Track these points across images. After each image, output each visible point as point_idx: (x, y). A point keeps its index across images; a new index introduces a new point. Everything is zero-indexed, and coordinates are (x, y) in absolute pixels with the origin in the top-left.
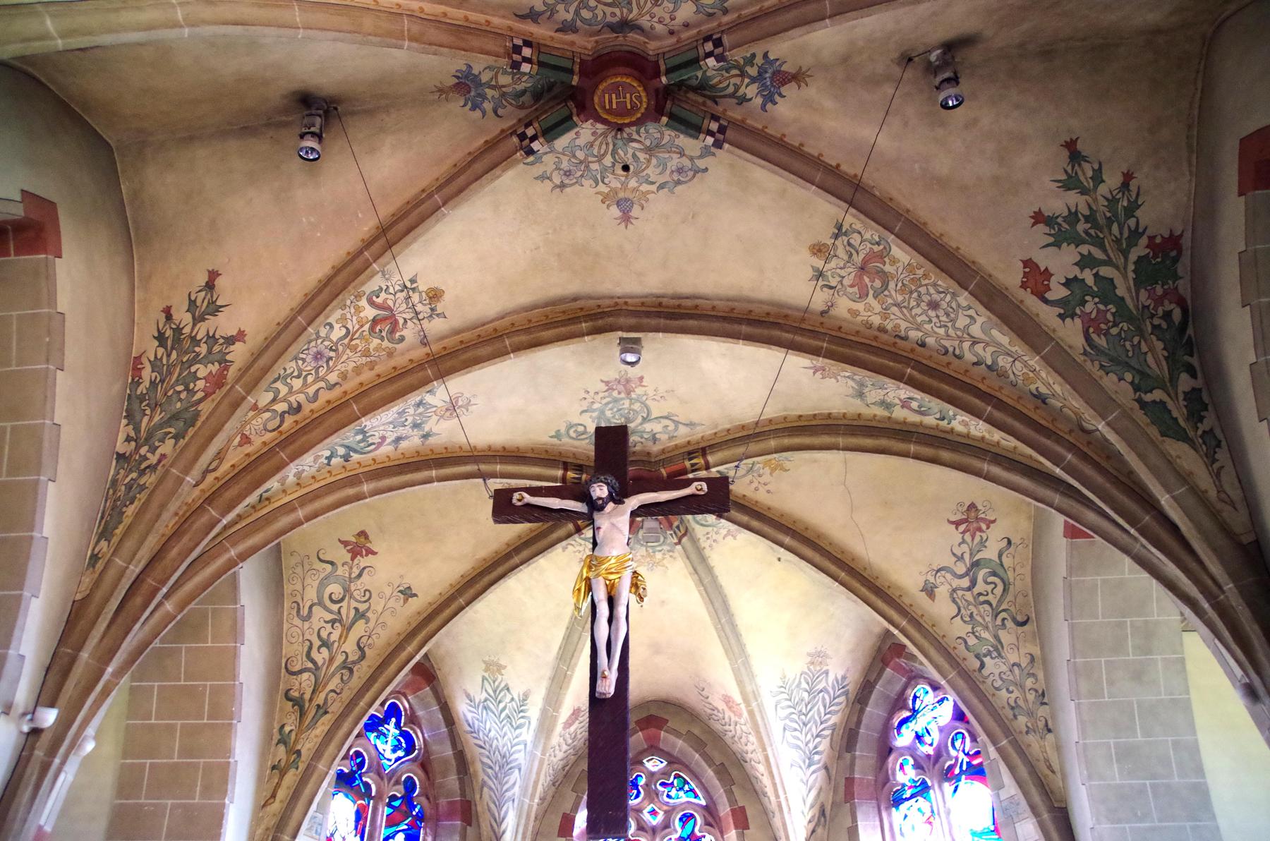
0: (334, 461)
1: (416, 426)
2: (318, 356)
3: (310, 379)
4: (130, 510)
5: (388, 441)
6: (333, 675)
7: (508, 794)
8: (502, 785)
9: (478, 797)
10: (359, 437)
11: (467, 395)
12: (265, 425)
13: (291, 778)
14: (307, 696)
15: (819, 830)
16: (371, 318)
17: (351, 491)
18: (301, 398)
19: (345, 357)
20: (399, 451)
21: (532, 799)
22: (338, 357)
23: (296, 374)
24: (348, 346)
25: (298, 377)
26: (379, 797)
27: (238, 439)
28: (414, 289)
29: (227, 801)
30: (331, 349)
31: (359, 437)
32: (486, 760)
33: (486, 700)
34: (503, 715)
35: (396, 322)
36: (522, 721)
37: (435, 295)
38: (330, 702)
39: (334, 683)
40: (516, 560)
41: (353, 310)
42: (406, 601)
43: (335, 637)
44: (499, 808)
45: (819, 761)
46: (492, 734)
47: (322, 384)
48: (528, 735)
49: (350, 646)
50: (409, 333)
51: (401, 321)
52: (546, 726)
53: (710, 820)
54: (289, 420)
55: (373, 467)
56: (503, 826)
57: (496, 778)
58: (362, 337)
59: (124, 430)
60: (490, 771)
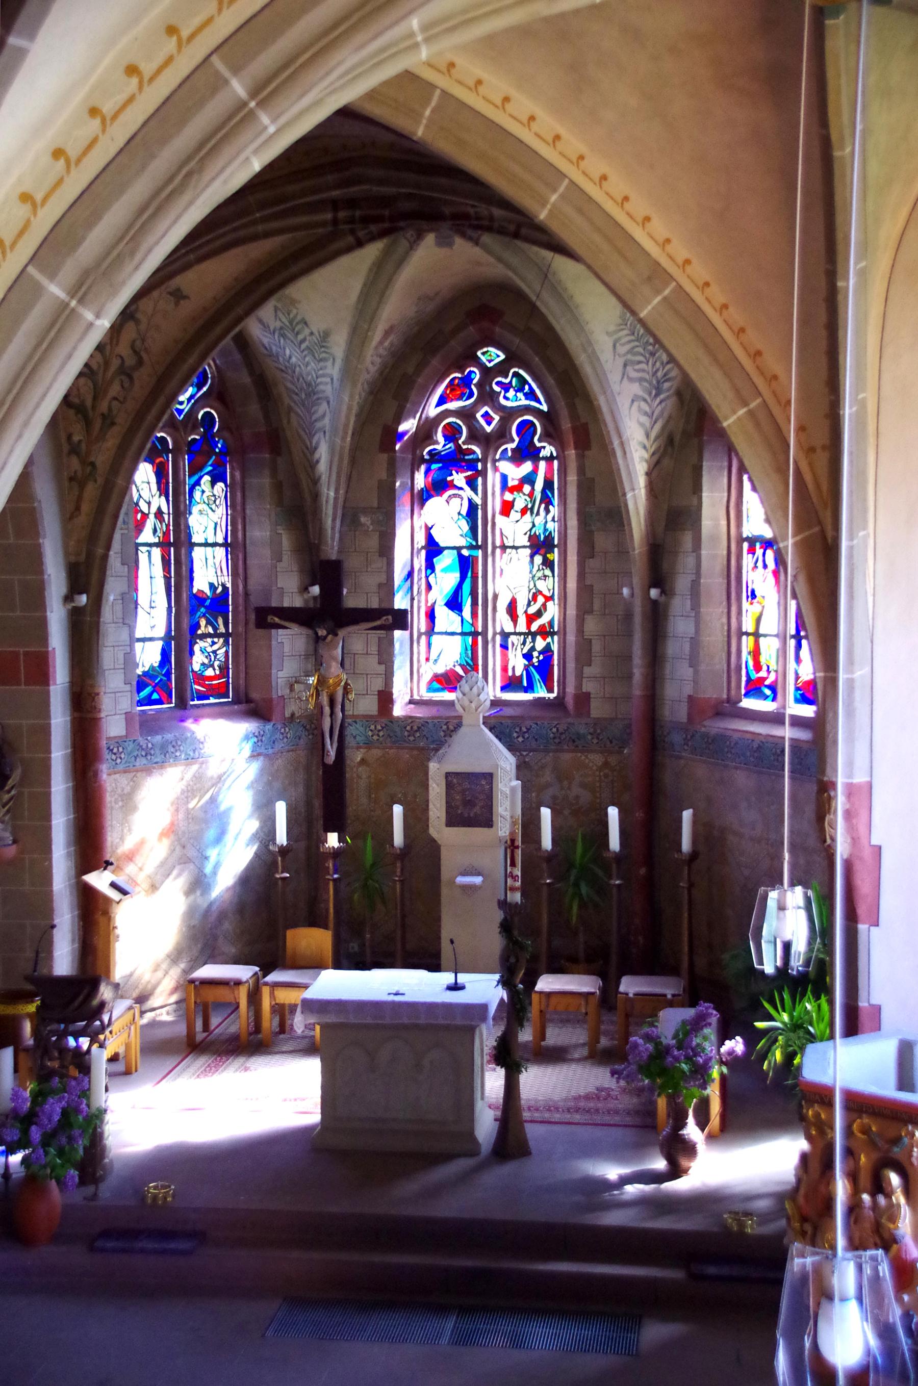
6: (111, 382)
7: (318, 425)
8: (311, 415)
9: (285, 422)
13: (91, 491)
14: (89, 403)
15: (666, 462)
21: (343, 439)
29: (41, 541)
32: (289, 385)
33: (281, 328)
34: (303, 346)
36: (324, 355)
38: (115, 412)
39: (115, 389)
40: (294, 269)
42: (177, 304)
44: (311, 436)
45: (668, 390)
46: (294, 360)
48: (334, 370)
52: (349, 371)
53: (551, 430)
56: (317, 456)
57: (303, 405)
60: (295, 397)
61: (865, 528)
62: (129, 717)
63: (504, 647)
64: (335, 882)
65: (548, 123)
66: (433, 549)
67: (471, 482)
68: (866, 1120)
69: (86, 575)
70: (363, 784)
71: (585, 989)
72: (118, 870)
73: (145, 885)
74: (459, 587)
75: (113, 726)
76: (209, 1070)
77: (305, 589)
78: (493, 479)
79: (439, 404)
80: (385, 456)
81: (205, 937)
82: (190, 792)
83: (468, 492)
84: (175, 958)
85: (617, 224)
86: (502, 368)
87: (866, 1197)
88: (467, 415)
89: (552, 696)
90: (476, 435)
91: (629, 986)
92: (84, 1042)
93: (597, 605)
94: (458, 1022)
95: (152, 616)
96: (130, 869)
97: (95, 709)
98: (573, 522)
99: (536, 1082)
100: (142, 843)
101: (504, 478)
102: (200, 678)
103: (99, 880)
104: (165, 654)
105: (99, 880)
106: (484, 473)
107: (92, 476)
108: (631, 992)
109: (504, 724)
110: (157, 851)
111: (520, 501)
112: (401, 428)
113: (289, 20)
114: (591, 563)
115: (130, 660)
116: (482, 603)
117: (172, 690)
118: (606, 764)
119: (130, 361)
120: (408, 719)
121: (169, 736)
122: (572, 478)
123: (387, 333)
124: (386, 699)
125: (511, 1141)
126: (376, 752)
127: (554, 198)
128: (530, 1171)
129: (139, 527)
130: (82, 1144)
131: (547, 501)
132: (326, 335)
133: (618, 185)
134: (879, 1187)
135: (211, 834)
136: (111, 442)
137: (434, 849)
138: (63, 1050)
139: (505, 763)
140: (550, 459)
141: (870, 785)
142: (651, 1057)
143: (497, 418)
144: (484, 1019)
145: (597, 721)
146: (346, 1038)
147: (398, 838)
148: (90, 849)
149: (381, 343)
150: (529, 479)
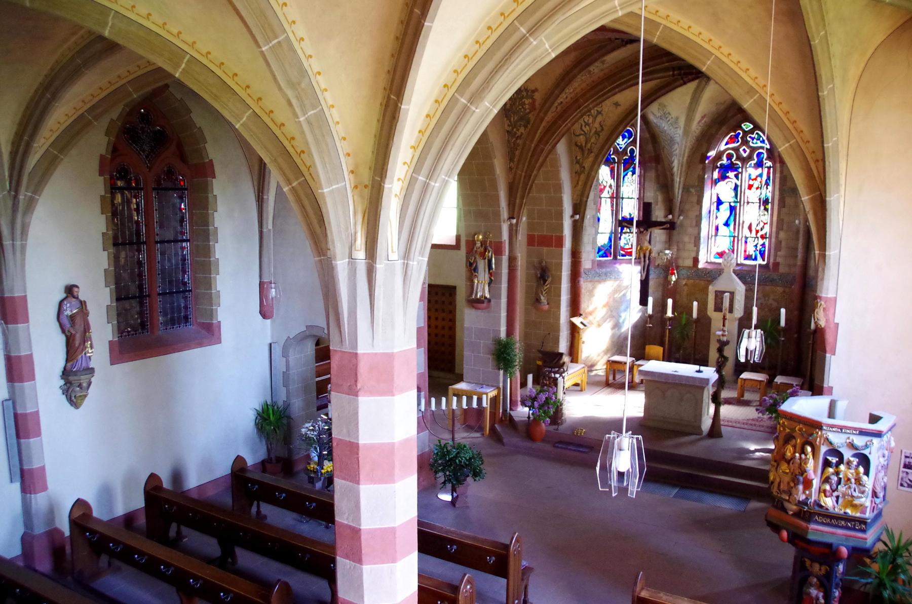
4: (517, 153)
13: (583, 177)
26: (619, 163)
39: (593, 140)
43: (590, 121)
48: (680, 132)
49: (597, 125)
52: (686, 132)
54: (559, 108)
59: (507, 122)
61: (838, 192)
62: (593, 262)
63: (746, 242)
64: (672, 330)
65: (706, 35)
66: (719, 202)
67: (736, 176)
68: (801, 426)
69: (579, 208)
70: (685, 293)
71: (760, 379)
72: (586, 318)
73: (596, 324)
74: (729, 218)
75: (586, 263)
76: (611, 393)
77: (666, 216)
78: (745, 175)
79: (726, 144)
80: (701, 166)
81: (618, 346)
82: (616, 291)
83: (735, 180)
84: (606, 352)
85: (736, 73)
86: (752, 131)
87: (797, 455)
88: (736, 150)
89: (765, 263)
90: (739, 158)
91: (779, 379)
92: (557, 376)
93: (785, 227)
94: (698, 385)
95: (606, 224)
96: (591, 318)
97: (579, 258)
98: (777, 193)
99: (726, 411)
100: (596, 309)
101: (750, 175)
102: (623, 249)
103: (577, 321)
104: (610, 239)
105: (577, 321)
106: (742, 173)
107: (583, 172)
108: (779, 382)
109: (744, 275)
110: (601, 312)
111: (756, 184)
112: (709, 154)
113: (540, 7)
114: (784, 210)
115: (594, 241)
116: (737, 225)
117: (612, 252)
118: (784, 291)
119: (599, 129)
120: (704, 269)
121: (608, 270)
122: (778, 175)
123: (703, 117)
124: (696, 261)
125: (715, 432)
126: (691, 281)
127: (709, 63)
128: (721, 443)
129: (602, 191)
130: (552, 411)
131: (767, 184)
132: (677, 118)
133: (735, 57)
134: (803, 451)
135: (623, 307)
136: (591, 159)
137: (709, 320)
138: (550, 378)
139: (740, 288)
140: (769, 168)
141: (836, 298)
142: (771, 405)
143: (748, 151)
144: (707, 384)
145: (781, 275)
146: (656, 386)
147: (695, 315)
148: (575, 309)
149: (700, 121)
150: (761, 175)
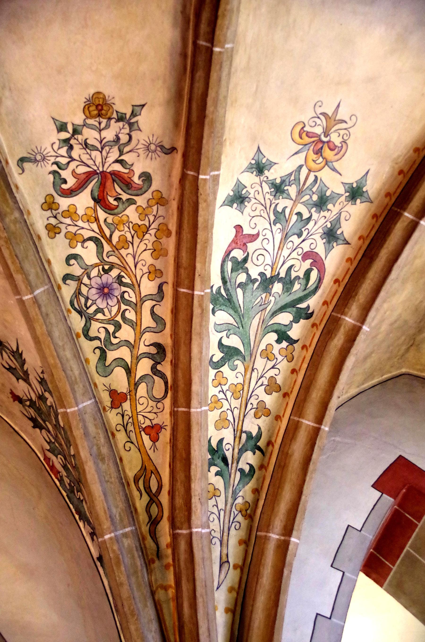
0: (295, 332)
1: (322, 203)
2: (105, 291)
3: (131, 315)
5: (320, 250)
10: (277, 287)
11: (306, 116)
12: (153, 398)
16: (92, 203)
17: (338, 341)
18: (149, 337)
19: (130, 260)
20: (354, 241)
22: (124, 267)
23: (111, 328)
24: (116, 249)
25: (118, 327)
27: (146, 438)
28: (76, 132)
30: (106, 272)
31: (277, 287)
35: (115, 175)
37: (98, 107)
41: (68, 221)
47: (148, 305)
50: (140, 164)
51: (118, 167)
55: (341, 289)
58: (113, 227)
